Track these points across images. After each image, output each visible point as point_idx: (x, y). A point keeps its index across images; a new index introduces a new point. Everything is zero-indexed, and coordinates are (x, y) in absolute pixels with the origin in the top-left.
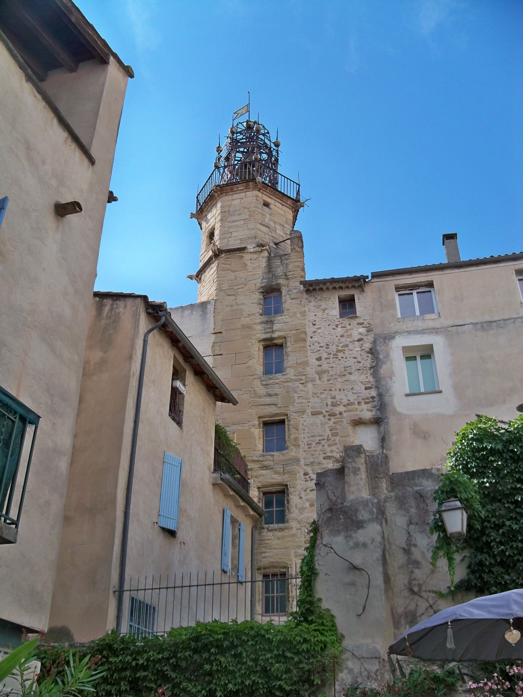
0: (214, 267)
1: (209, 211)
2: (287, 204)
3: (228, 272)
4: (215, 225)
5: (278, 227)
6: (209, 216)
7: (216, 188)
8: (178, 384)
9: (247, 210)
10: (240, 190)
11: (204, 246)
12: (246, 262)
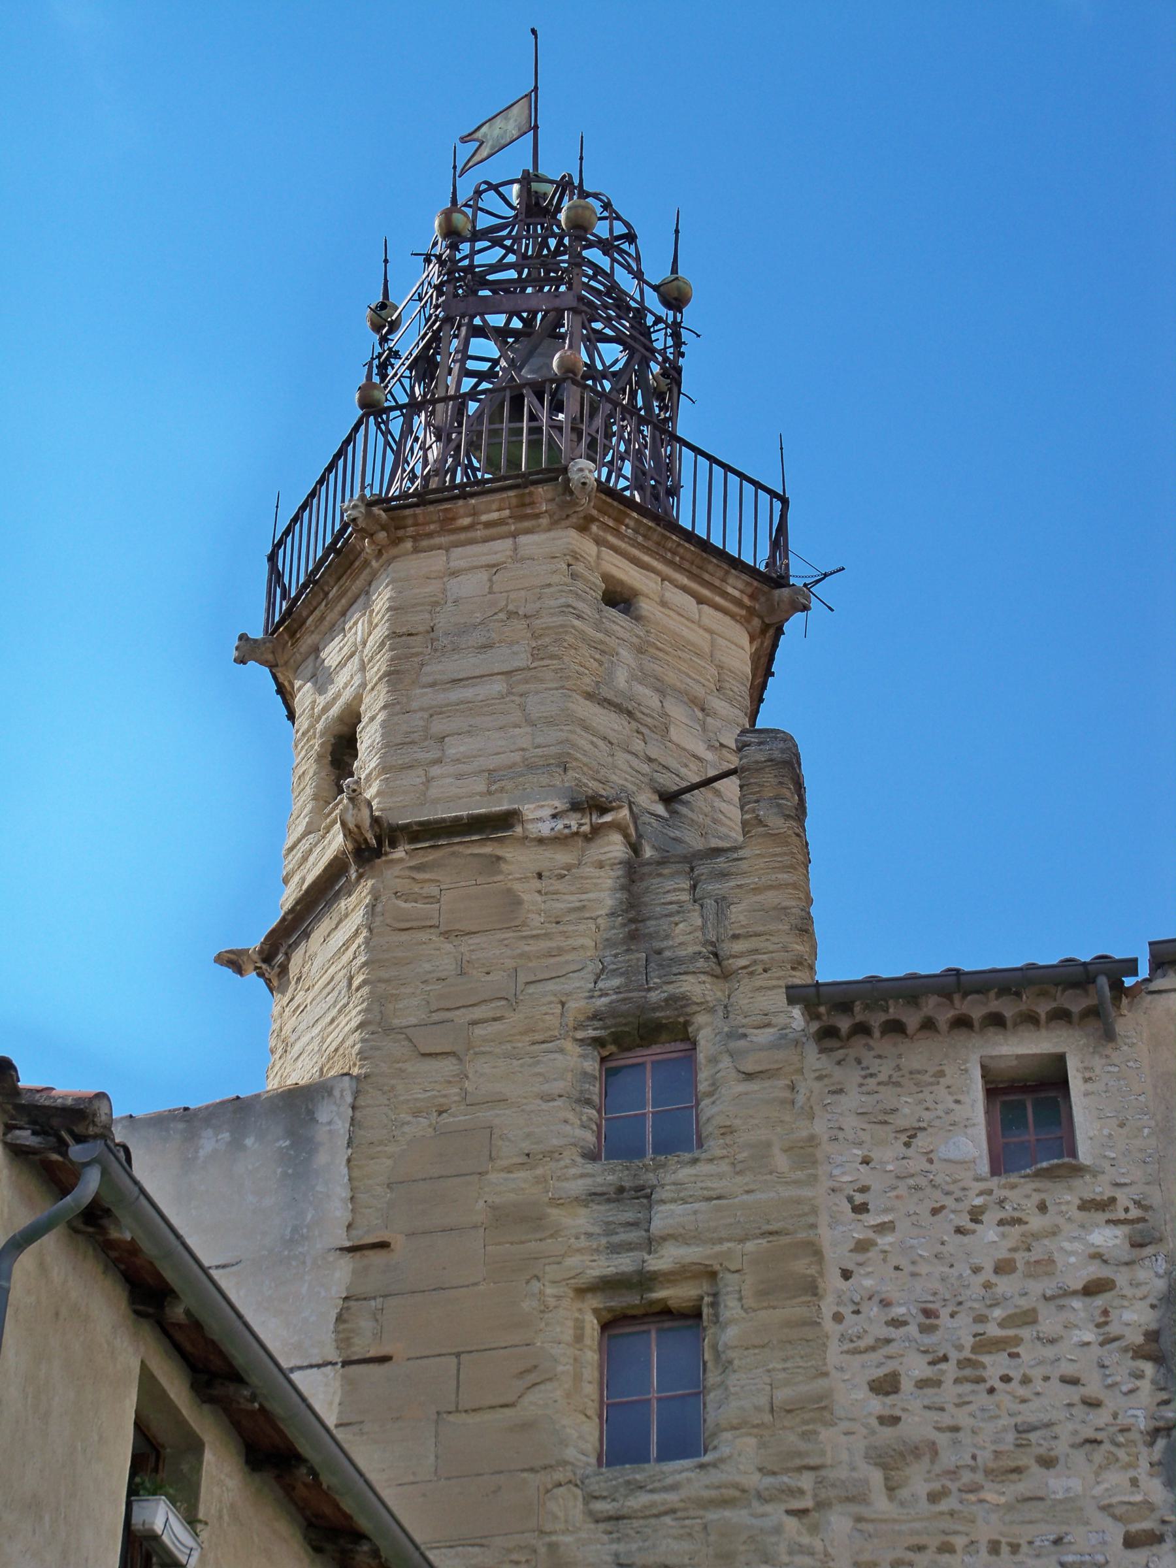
1: (334, 630)
2: (724, 594)
3: (423, 936)
4: (358, 698)
5: (677, 711)
6: (332, 654)
7: (369, 514)
8: (161, 1517)
9: (520, 625)
10: (489, 525)
11: (302, 804)
12: (517, 886)
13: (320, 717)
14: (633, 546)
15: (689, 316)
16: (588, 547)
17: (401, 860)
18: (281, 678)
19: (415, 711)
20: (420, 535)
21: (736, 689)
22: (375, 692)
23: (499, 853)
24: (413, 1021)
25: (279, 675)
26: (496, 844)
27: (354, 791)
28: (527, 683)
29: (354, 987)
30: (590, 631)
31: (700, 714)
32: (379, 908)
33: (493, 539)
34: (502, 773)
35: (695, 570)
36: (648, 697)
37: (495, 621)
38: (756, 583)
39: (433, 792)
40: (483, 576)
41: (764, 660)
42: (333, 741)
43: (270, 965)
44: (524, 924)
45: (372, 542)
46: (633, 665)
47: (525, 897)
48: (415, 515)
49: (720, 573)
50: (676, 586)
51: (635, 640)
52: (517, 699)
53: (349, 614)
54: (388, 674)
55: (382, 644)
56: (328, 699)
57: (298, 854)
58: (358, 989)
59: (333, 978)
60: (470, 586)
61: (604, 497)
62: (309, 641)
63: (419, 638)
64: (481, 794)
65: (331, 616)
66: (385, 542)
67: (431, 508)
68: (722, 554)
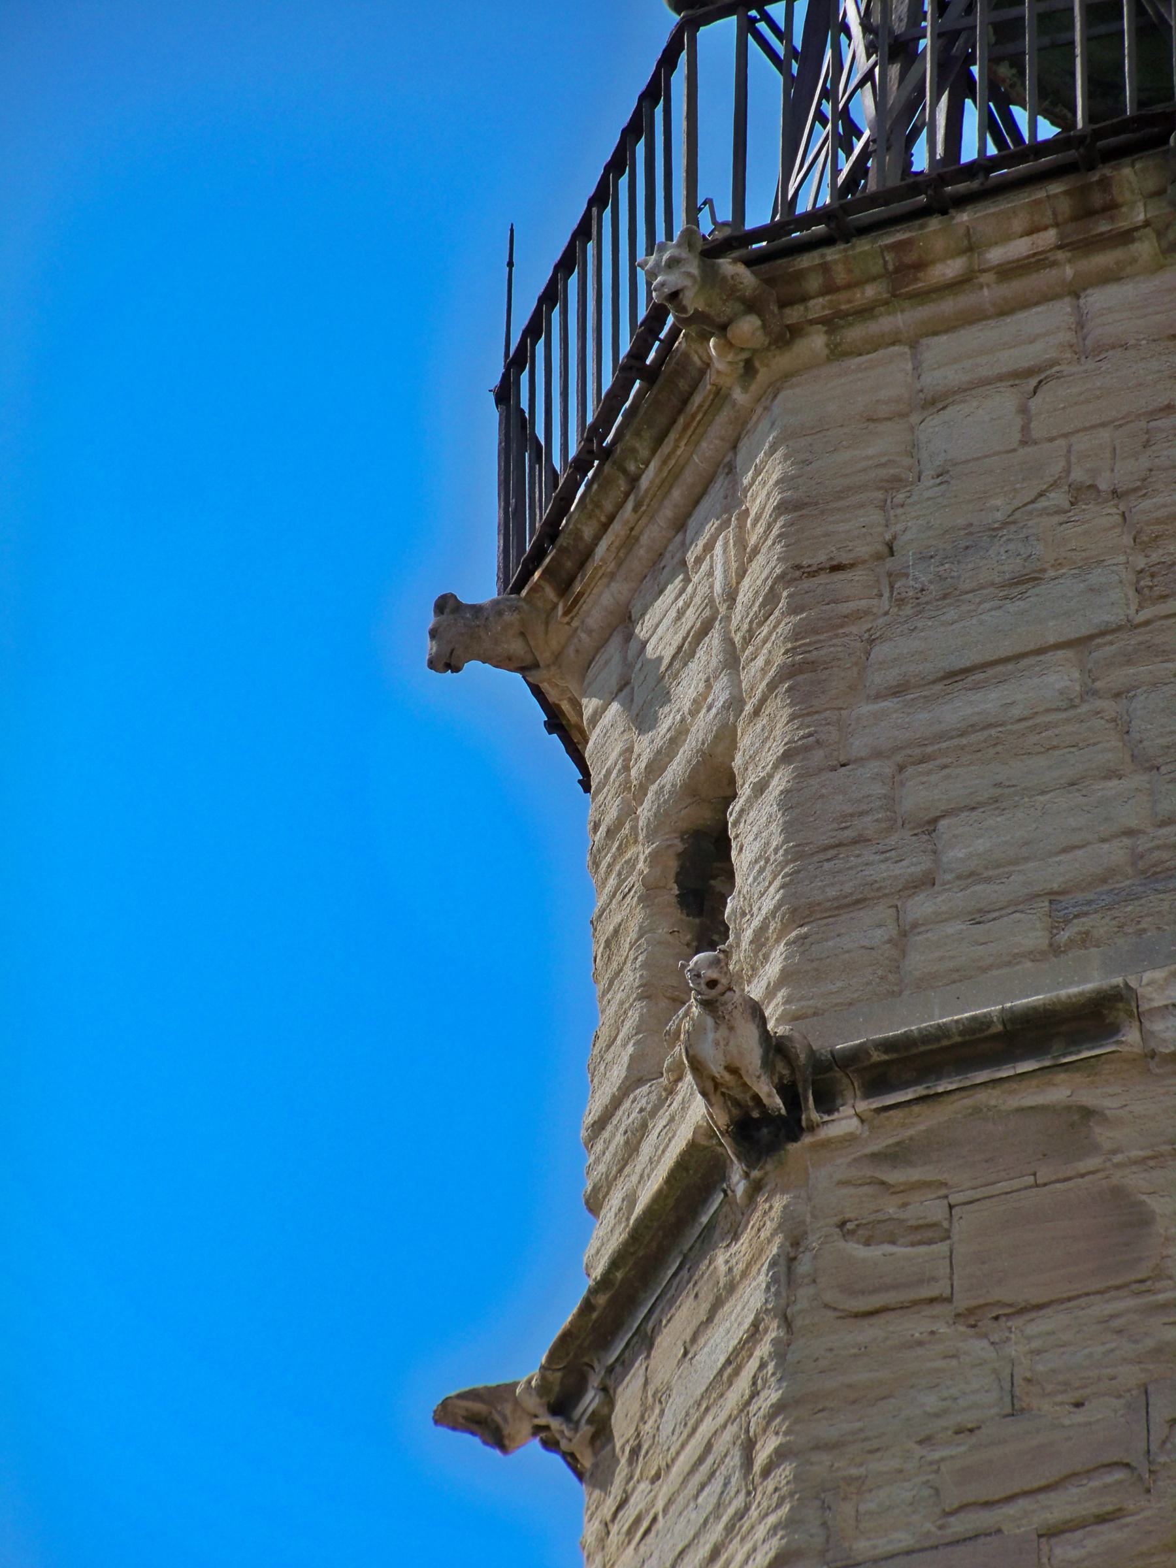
0: (742, 1267)
1: (663, 566)
3: (914, 1326)
4: (726, 736)
6: (661, 628)
7: (710, 277)
9: (1103, 516)
10: (1007, 271)
11: (614, 1012)
12: (1135, 1180)
13: (643, 789)
17: (850, 1139)
18: (553, 696)
19: (860, 761)
20: (844, 315)
22: (763, 721)
23: (1088, 1098)
24: (903, 1539)
25: (545, 686)
26: (1078, 1078)
27: (712, 984)
28: (1129, 662)
29: (757, 1468)
32: (804, 1266)
33: (1024, 304)
34: (1080, 896)
37: (1045, 512)
39: (918, 961)
40: (1005, 402)
42: (680, 847)
43: (568, 1419)
44: (1159, 1274)
45: (728, 345)
47: (1156, 1205)
48: (825, 268)
52: (1108, 706)
53: (692, 523)
54: (789, 672)
55: (771, 598)
56: (659, 742)
57: (615, 1137)
58: (766, 1472)
59: (708, 1448)
60: (976, 428)
62: (607, 599)
63: (858, 576)
64: (1034, 956)
65: (652, 534)
66: (761, 339)
67: (863, 245)
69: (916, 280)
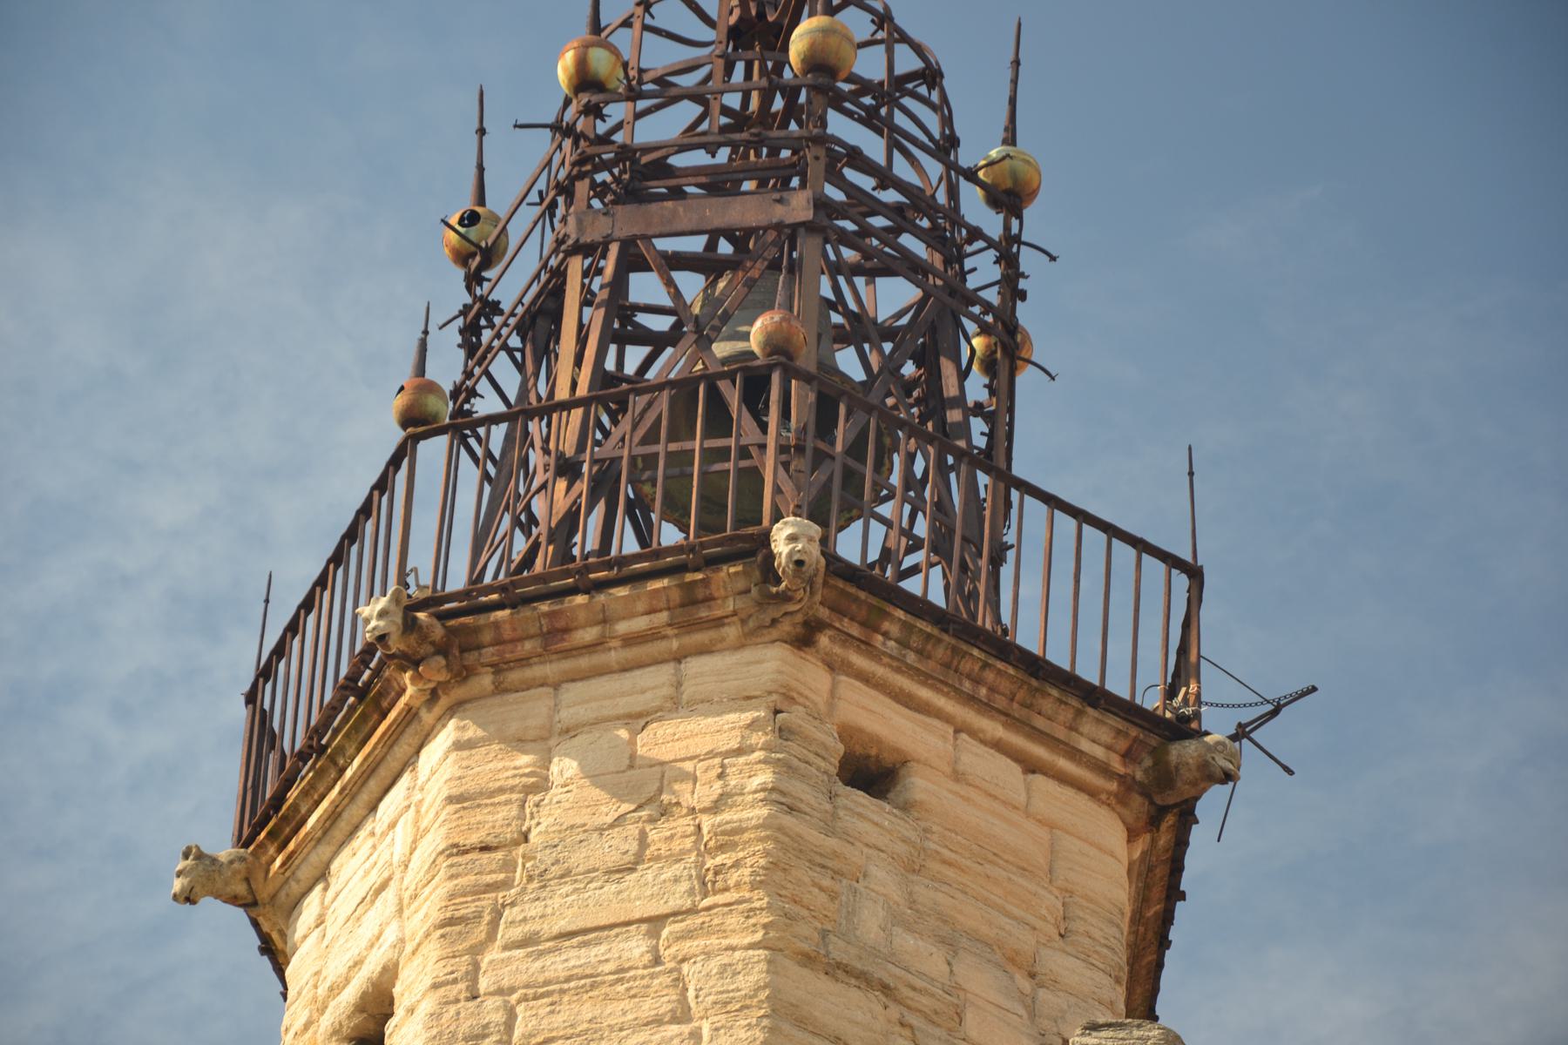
2: (1074, 754)
7: (410, 625)
10: (630, 641)
14: (898, 670)
15: (1035, 222)
16: (812, 676)
18: (266, 928)
21: (1097, 934)
25: (261, 920)
30: (814, 836)
31: (1026, 985)
33: (641, 665)
35: (1016, 710)
36: (922, 955)
38: (1134, 732)
41: (1161, 872)
46: (896, 895)
49: (1066, 715)
50: (983, 742)
51: (901, 848)
61: (841, 584)
68: (1068, 681)
69: (563, 640)
